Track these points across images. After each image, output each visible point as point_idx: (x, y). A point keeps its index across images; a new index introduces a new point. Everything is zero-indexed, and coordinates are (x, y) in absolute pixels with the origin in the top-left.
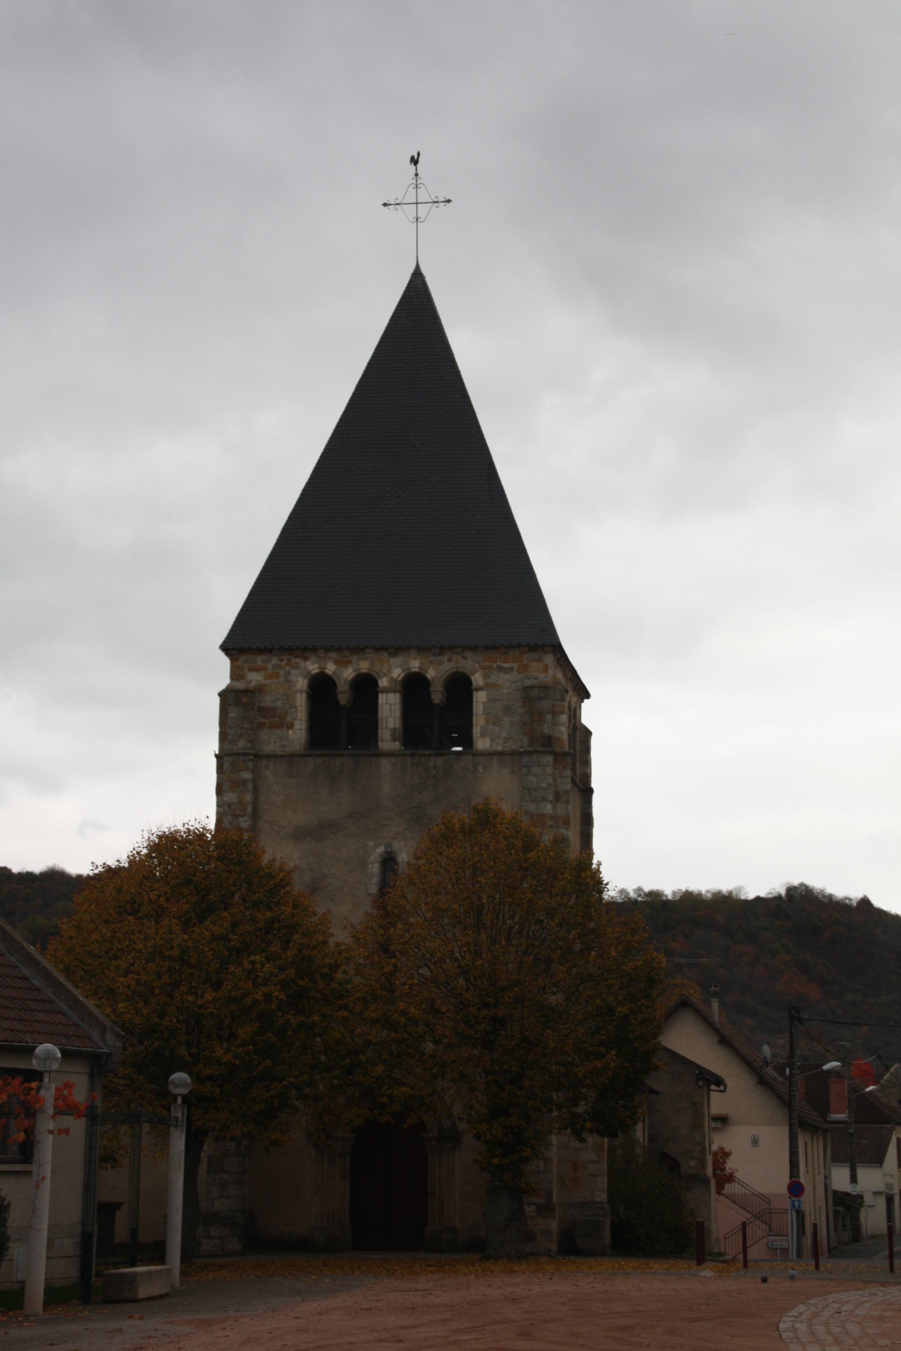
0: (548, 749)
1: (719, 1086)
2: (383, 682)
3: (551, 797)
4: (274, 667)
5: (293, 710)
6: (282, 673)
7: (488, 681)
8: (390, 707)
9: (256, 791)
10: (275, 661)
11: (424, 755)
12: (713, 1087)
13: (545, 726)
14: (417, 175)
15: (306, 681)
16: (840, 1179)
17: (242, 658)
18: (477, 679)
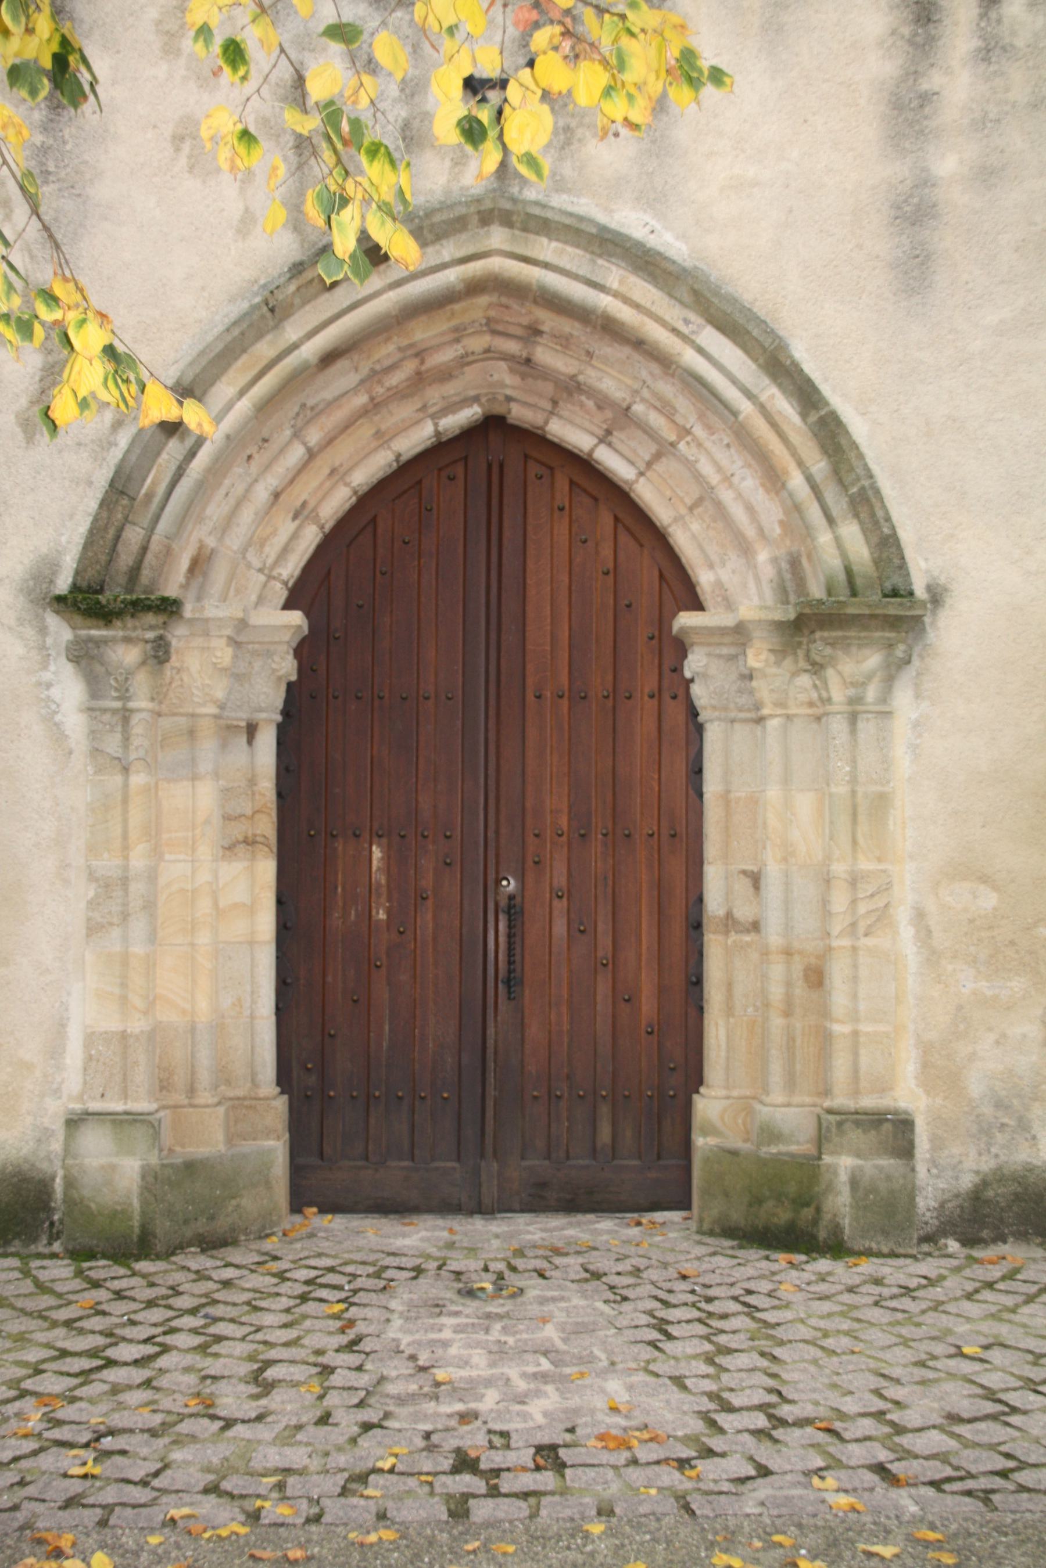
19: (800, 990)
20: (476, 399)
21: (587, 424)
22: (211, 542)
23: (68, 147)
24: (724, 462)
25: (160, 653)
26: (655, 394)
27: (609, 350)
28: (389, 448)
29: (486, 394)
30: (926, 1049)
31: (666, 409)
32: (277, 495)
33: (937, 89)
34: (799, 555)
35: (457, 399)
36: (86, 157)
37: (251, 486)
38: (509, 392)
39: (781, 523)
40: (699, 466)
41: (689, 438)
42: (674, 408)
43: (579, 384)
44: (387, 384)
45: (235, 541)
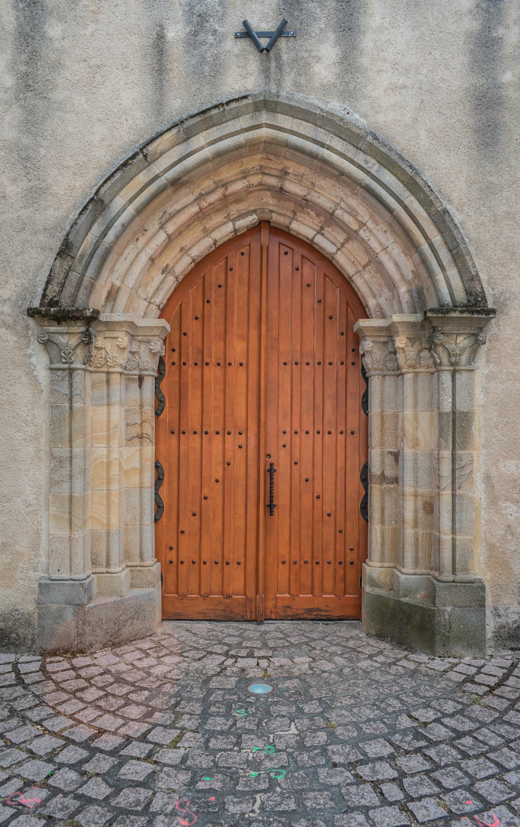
19: (421, 514)
20: (255, 211)
21: (311, 224)
22: (118, 283)
23: (40, 72)
24: (384, 241)
25: (87, 340)
26: (347, 205)
27: (323, 182)
28: (210, 237)
29: (259, 209)
30: (491, 547)
31: (353, 213)
32: (152, 260)
33: (501, 36)
34: (422, 289)
35: (244, 211)
36: (49, 77)
37: (138, 254)
38: (271, 208)
39: (413, 272)
40: (370, 243)
41: (365, 228)
42: (357, 212)
43: (307, 200)
44: (208, 201)
45: (131, 281)
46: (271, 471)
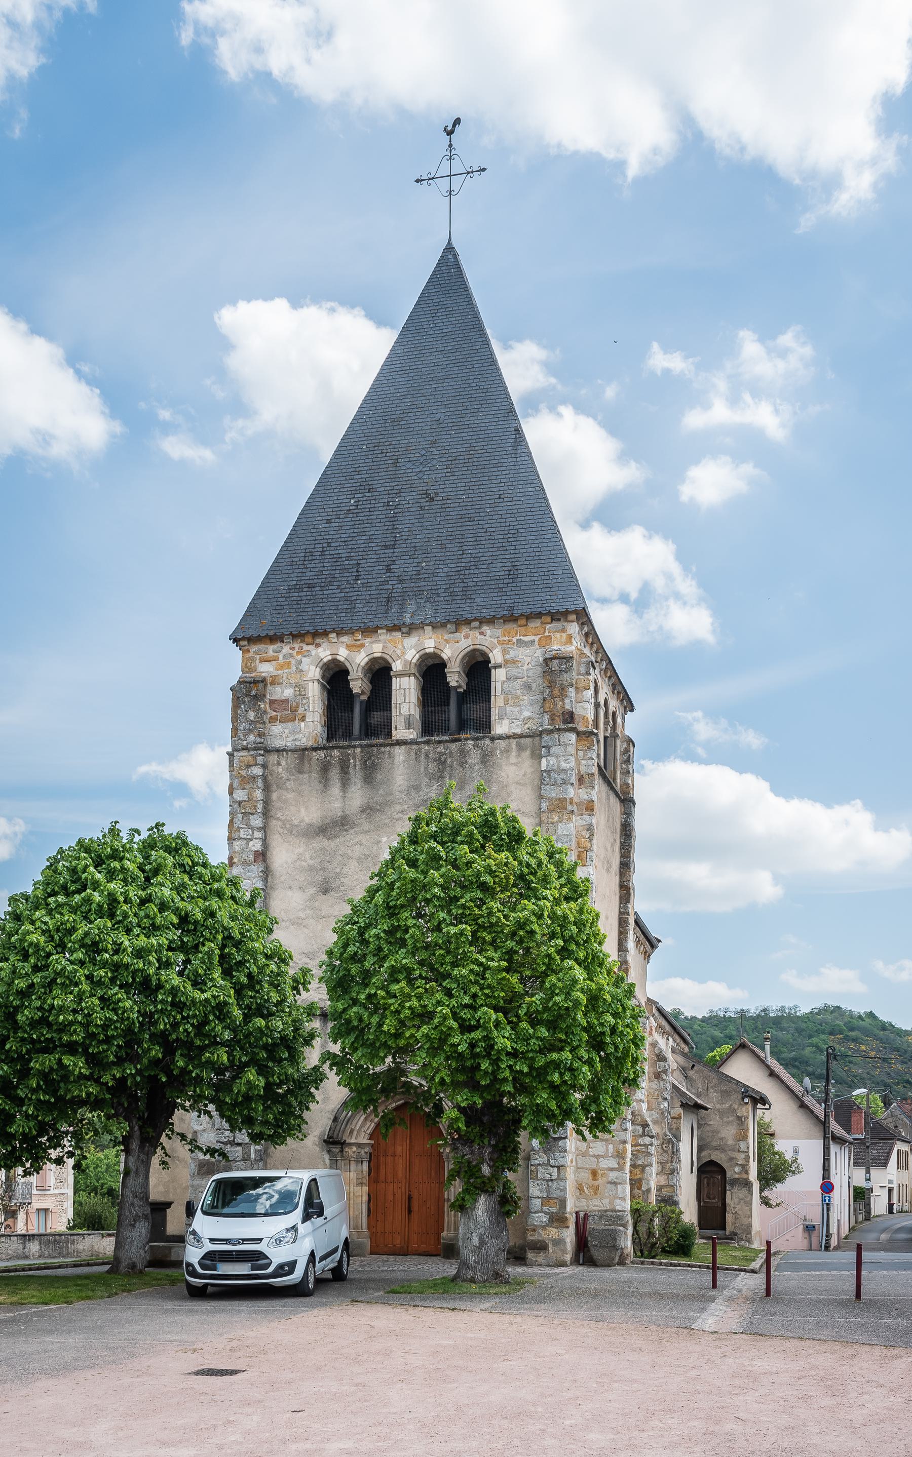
0: (570, 726)
1: (764, 1105)
2: (397, 666)
3: (574, 779)
4: (285, 656)
5: (304, 701)
6: (293, 661)
7: (508, 657)
8: (406, 695)
9: (267, 788)
10: (286, 649)
11: (439, 742)
12: (759, 1106)
13: (567, 701)
14: (450, 146)
15: (318, 669)
16: (859, 1177)
17: (254, 648)
18: (496, 656)
46: (410, 1198)
